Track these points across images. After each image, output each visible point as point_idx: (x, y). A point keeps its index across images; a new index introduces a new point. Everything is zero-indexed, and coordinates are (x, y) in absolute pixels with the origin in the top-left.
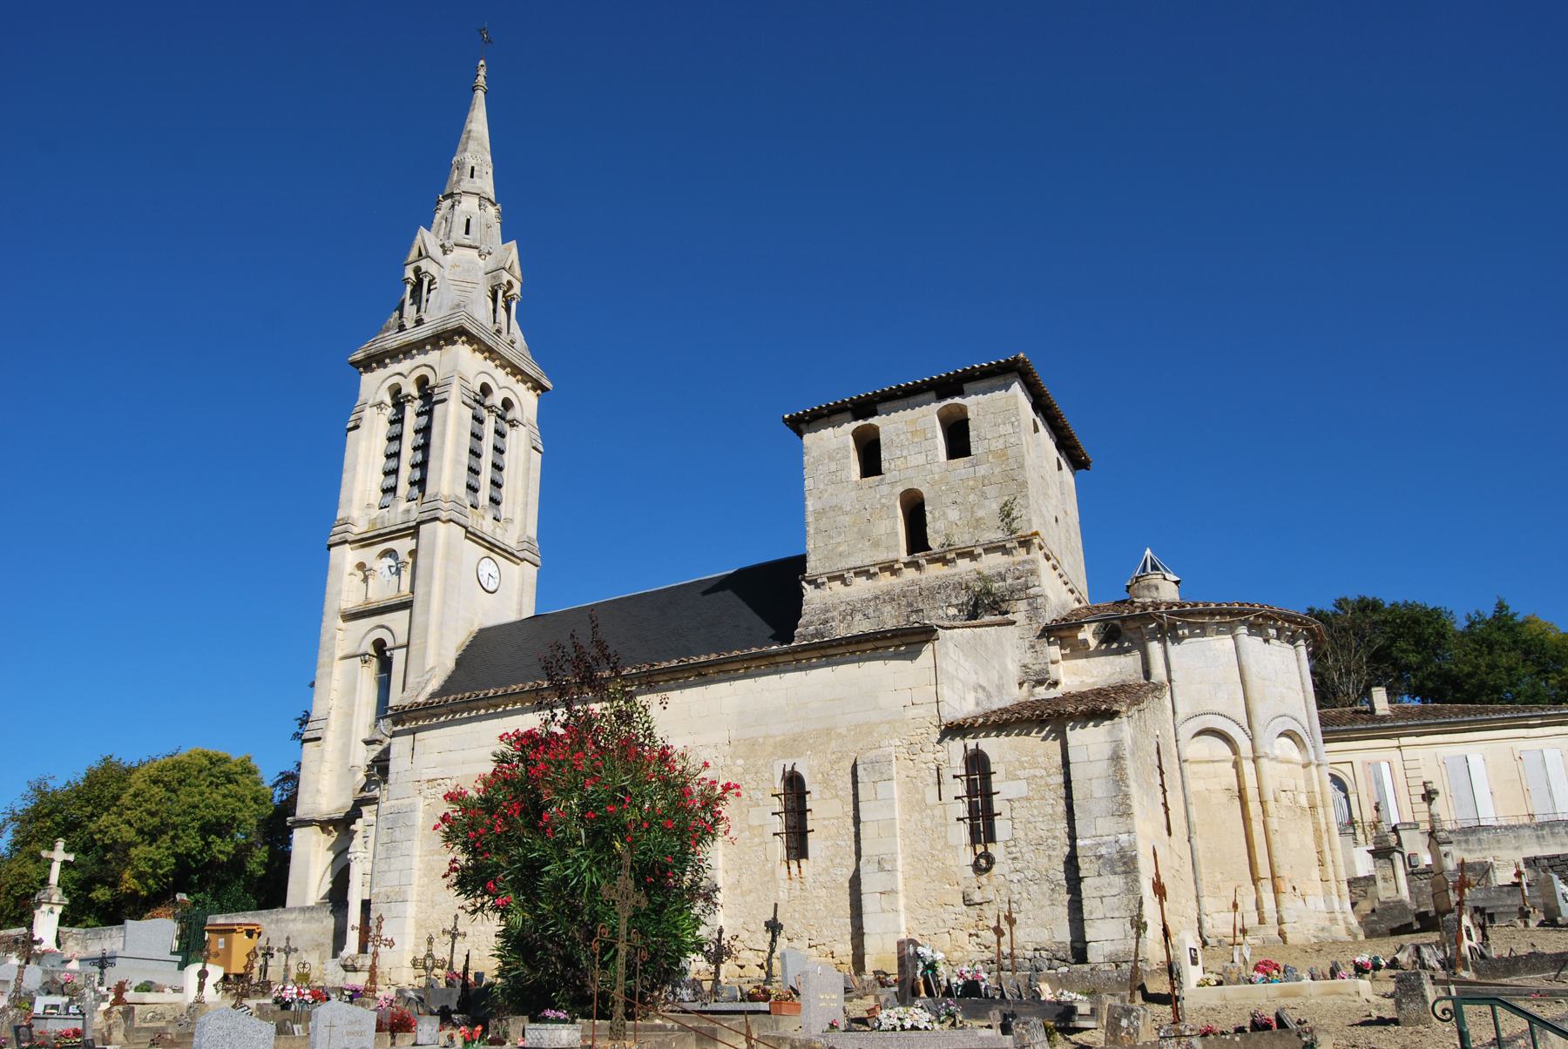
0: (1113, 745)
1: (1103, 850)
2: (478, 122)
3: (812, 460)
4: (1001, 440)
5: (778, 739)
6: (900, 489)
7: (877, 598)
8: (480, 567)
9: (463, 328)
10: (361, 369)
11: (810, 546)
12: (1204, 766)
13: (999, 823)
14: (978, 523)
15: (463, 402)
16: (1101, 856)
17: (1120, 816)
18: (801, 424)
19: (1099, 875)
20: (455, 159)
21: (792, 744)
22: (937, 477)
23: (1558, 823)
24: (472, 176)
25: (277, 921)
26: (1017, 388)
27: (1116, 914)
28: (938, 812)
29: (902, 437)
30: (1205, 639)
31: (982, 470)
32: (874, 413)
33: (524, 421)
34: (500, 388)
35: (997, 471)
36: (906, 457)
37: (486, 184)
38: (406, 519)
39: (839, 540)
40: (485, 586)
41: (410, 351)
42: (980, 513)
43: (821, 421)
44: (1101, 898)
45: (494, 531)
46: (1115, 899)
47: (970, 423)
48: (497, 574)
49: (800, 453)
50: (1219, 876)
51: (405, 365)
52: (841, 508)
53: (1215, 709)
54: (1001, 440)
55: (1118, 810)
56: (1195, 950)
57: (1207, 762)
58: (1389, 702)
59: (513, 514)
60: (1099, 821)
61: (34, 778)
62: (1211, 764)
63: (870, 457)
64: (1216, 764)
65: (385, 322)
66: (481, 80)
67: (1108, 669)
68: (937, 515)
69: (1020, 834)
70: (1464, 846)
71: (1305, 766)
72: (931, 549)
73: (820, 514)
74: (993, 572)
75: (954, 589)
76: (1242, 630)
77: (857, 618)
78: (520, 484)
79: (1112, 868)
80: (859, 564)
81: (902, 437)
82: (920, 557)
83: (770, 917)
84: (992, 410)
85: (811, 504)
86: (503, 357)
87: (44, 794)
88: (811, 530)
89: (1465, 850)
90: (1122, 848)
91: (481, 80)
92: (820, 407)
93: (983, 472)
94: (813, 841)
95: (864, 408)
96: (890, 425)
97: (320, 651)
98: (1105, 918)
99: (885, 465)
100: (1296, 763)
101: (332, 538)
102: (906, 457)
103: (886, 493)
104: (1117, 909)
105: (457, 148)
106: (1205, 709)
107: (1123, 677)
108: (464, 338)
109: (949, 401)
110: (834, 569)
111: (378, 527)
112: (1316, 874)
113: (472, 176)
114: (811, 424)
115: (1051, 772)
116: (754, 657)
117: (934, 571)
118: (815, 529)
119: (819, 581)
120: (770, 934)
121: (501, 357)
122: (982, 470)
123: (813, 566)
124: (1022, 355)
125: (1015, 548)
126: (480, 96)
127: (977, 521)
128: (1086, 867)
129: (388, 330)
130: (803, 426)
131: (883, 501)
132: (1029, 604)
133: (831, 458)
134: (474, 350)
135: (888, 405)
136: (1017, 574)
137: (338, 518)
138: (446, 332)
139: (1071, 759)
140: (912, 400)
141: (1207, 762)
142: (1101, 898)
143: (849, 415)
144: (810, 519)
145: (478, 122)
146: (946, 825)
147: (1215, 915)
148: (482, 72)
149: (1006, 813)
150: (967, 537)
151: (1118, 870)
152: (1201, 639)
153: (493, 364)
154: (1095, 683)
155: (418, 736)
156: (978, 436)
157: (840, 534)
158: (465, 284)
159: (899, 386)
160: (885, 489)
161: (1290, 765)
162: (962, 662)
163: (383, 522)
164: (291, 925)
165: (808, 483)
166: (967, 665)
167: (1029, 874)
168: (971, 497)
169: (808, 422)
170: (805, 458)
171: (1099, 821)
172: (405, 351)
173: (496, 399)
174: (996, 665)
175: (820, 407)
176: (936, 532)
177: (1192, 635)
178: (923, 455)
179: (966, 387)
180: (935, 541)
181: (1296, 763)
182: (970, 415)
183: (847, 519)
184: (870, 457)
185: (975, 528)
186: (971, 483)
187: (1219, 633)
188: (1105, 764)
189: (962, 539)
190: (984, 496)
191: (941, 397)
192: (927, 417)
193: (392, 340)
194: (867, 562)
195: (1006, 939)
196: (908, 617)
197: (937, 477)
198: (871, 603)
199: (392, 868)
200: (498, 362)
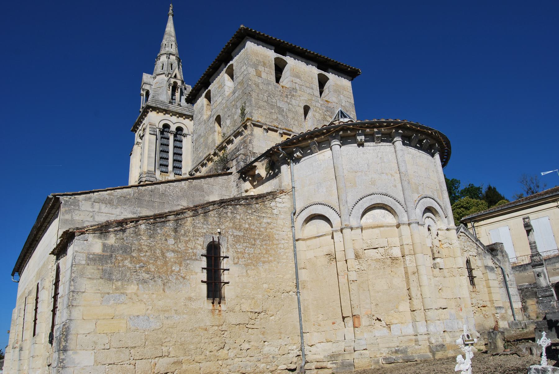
2: (170, 28)
9: (148, 106)
12: (314, 240)
15: (150, 134)
26: (250, 45)
30: (313, 155)
33: (190, 133)
34: (174, 124)
37: (174, 49)
50: (321, 317)
53: (317, 201)
57: (315, 237)
62: (318, 239)
64: (321, 238)
66: (171, 11)
71: (398, 226)
76: (335, 143)
86: (172, 111)
91: (171, 11)
100: (391, 226)
106: (312, 202)
108: (151, 109)
112: (405, 307)
119: (192, 174)
121: (172, 112)
124: (242, 26)
125: (243, 131)
126: (171, 17)
134: (158, 113)
135: (212, 78)
139: (320, 238)
141: (315, 237)
145: (170, 28)
147: (318, 345)
148: (171, 9)
152: (311, 156)
153: (169, 116)
156: (236, 77)
161: (382, 229)
173: (173, 128)
177: (304, 155)
181: (391, 226)
187: (320, 148)
200: (171, 114)
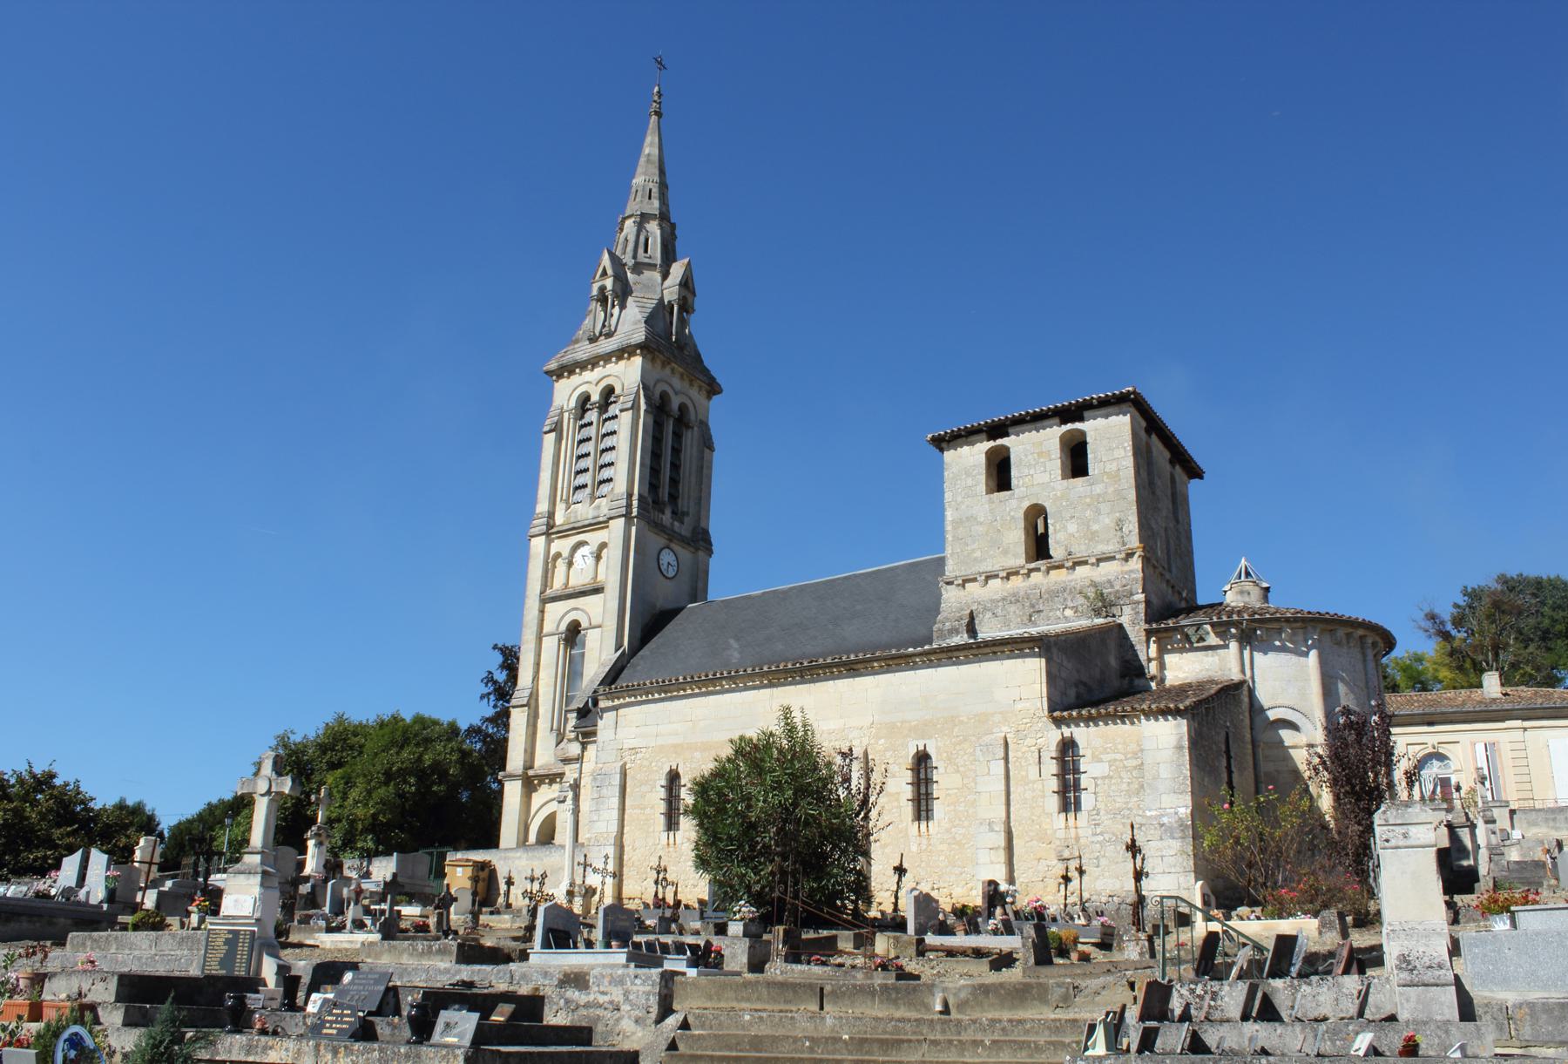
0: (1178, 737)
1: (1165, 820)
3: (951, 475)
4: (1115, 464)
5: (913, 723)
6: (1026, 504)
7: (1004, 599)
8: (661, 557)
10: (554, 378)
11: (948, 551)
13: (1084, 796)
14: (1093, 537)
16: (1162, 825)
17: (1181, 793)
18: (942, 442)
19: (1161, 839)
20: (634, 181)
21: (677, 749)
22: (1059, 494)
23: (1562, 810)
24: (650, 198)
25: (505, 858)
27: (1173, 870)
28: (1038, 786)
29: (1030, 457)
31: (1098, 489)
32: (1081, 419)
35: (1111, 490)
36: (1032, 476)
38: (596, 515)
39: (974, 547)
40: (665, 573)
41: (598, 363)
42: (1095, 527)
43: (960, 441)
44: (1162, 857)
45: (672, 524)
46: (1173, 858)
47: (1089, 447)
48: (675, 563)
49: (940, 468)
51: (588, 375)
52: (976, 519)
54: (1115, 464)
55: (1179, 789)
56: (1208, 896)
58: (1502, 685)
59: (688, 508)
60: (1164, 797)
61: (280, 732)
63: (1000, 474)
65: (574, 335)
67: (1197, 667)
68: (1058, 527)
69: (1101, 806)
70: (1551, 824)
72: (1051, 557)
73: (958, 523)
74: (1105, 579)
75: (1071, 592)
77: (987, 616)
78: (693, 480)
79: (1172, 833)
80: (989, 569)
81: (1030, 457)
82: (1042, 564)
83: (897, 864)
84: (1108, 436)
85: (950, 515)
87: (285, 746)
88: (949, 537)
89: (1552, 828)
90: (1180, 819)
92: (959, 429)
93: (1098, 491)
94: (938, 808)
95: (997, 430)
96: (1018, 444)
97: (524, 629)
98: (1164, 873)
99: (1014, 482)
101: (533, 530)
102: (1032, 476)
103: (1014, 504)
104: (1175, 866)
105: (635, 170)
107: (1210, 673)
109: (1069, 426)
110: (969, 572)
111: (572, 520)
113: (650, 198)
114: (951, 443)
115: (1129, 756)
116: (893, 658)
117: (1058, 576)
118: (953, 537)
120: (897, 876)
122: (1098, 489)
123: (951, 569)
127: (1092, 533)
128: (1405, 827)
129: (577, 341)
130: (944, 445)
131: (1012, 514)
132: (1133, 609)
133: (968, 474)
135: (1018, 428)
136: (1124, 582)
137: (537, 511)
138: (630, 346)
140: (1039, 425)
142: (1162, 857)
143: (984, 436)
144: (949, 528)
146: (1044, 797)
149: (1091, 789)
150: (1083, 547)
151: (1176, 835)
154: (1187, 678)
155: (621, 711)
156: (1095, 458)
157: (974, 543)
158: (645, 300)
159: (1028, 413)
160: (1014, 503)
162: (1065, 663)
163: (576, 517)
164: (517, 862)
165: (948, 496)
166: (1070, 666)
167: (1107, 836)
168: (1088, 513)
169: (949, 441)
170: (946, 474)
171: (1164, 797)
172: (593, 363)
174: (1099, 664)
175: (959, 429)
176: (1057, 543)
178: (1047, 473)
179: (1086, 414)
180: (1056, 551)
182: (1088, 439)
183: (981, 529)
184: (1000, 474)
185: (1090, 540)
186: (1088, 500)
188: (1170, 752)
189: (1080, 551)
190: (1098, 512)
191: (1064, 422)
192: (1051, 436)
193: (583, 351)
194: (996, 567)
195: (1074, 885)
196: (1031, 616)
197: (1059, 494)
198: (1000, 604)
199: (601, 818)
